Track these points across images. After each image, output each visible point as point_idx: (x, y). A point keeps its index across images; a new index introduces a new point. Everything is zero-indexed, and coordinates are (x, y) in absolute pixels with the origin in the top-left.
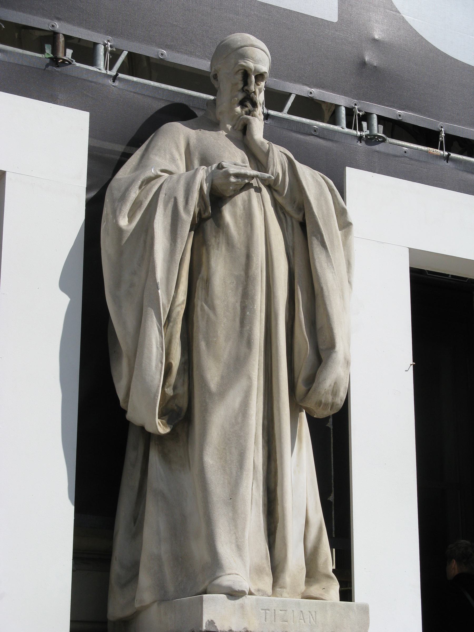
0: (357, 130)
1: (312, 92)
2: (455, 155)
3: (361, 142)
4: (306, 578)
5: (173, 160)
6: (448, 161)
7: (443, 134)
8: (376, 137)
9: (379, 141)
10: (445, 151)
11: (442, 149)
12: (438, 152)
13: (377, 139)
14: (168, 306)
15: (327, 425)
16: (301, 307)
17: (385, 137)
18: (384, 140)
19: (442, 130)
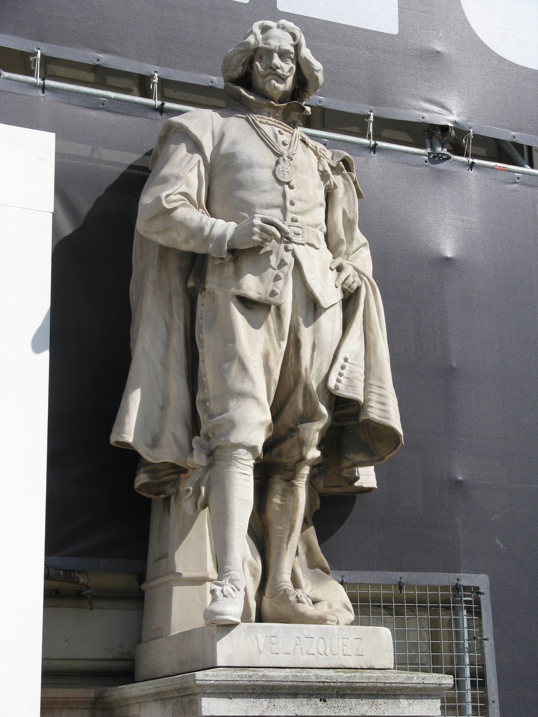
0: (371, 139)
1: (100, 59)
2: (389, 145)
3: (471, 170)
4: (47, 581)
5: (188, 185)
6: (473, 169)
7: (156, 80)
8: (440, 155)
9: (443, 159)
10: (373, 140)
11: (369, 138)
12: (365, 141)
13: (441, 157)
14: (277, 366)
15: (376, 487)
16: (273, 332)
17: (449, 155)
18: (449, 158)
19: (370, 114)
